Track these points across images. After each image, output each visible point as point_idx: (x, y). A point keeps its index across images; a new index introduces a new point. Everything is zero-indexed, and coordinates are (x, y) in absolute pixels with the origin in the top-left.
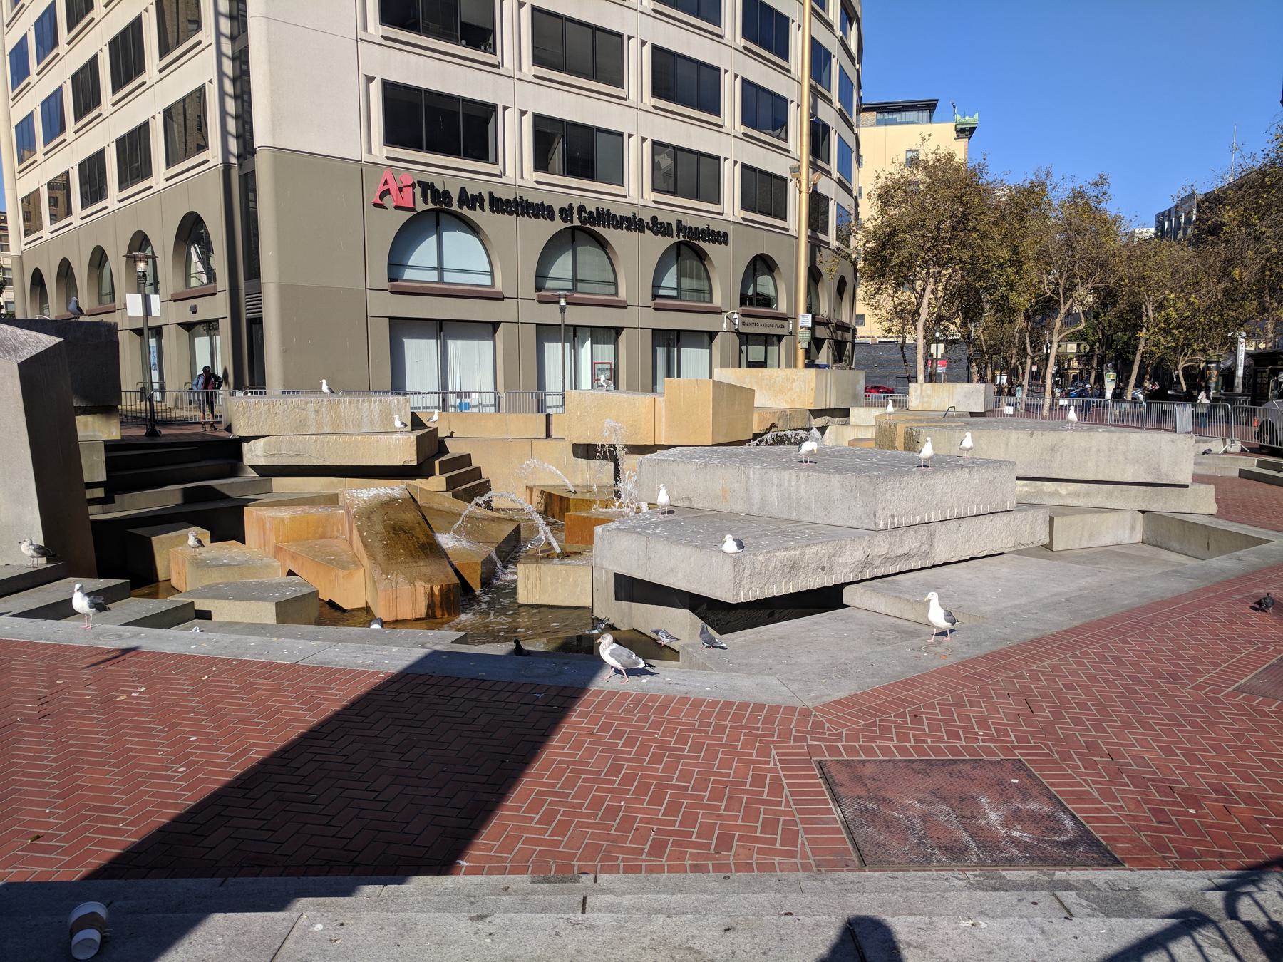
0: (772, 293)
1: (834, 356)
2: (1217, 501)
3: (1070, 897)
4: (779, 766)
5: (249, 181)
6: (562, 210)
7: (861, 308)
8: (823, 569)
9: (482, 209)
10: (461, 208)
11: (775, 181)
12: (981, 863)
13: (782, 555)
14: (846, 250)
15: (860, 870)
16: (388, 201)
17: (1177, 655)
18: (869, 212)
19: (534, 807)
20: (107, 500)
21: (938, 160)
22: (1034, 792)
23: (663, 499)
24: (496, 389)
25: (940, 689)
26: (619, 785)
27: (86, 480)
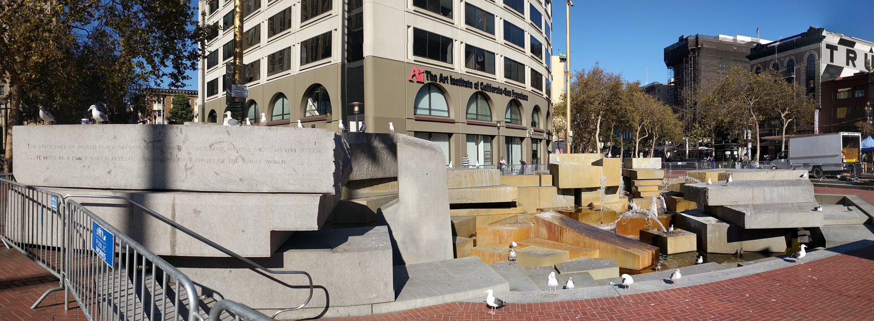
6: (475, 84)
9: (447, 82)
16: (414, 79)
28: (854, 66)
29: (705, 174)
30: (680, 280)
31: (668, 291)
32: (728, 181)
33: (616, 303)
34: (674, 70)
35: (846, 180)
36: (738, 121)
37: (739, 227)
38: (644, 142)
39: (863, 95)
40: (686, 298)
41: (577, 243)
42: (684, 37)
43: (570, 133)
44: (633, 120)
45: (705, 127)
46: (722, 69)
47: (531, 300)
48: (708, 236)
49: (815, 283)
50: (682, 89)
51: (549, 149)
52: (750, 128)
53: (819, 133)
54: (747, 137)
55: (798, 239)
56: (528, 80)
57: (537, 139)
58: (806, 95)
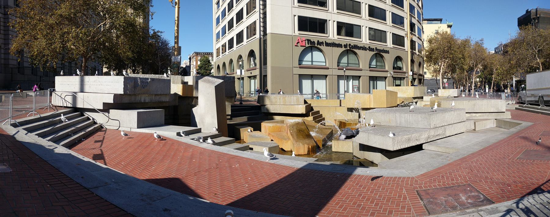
0: (401, 66)
1: (419, 83)
2: (511, 116)
3: (482, 213)
4: (406, 192)
5: (265, 41)
6: (344, 45)
7: (425, 70)
8: (417, 140)
10: (318, 45)
11: (401, 37)
12: (461, 209)
13: (406, 137)
14: (421, 55)
15: (428, 216)
16: (299, 45)
17: (505, 153)
18: (426, 45)
19: (337, 204)
20: (231, 119)
21: (443, 33)
22: (473, 191)
23: (372, 123)
24: (326, 93)
25: (448, 169)
26: (361, 199)
27: (227, 114)
42: (529, 11)
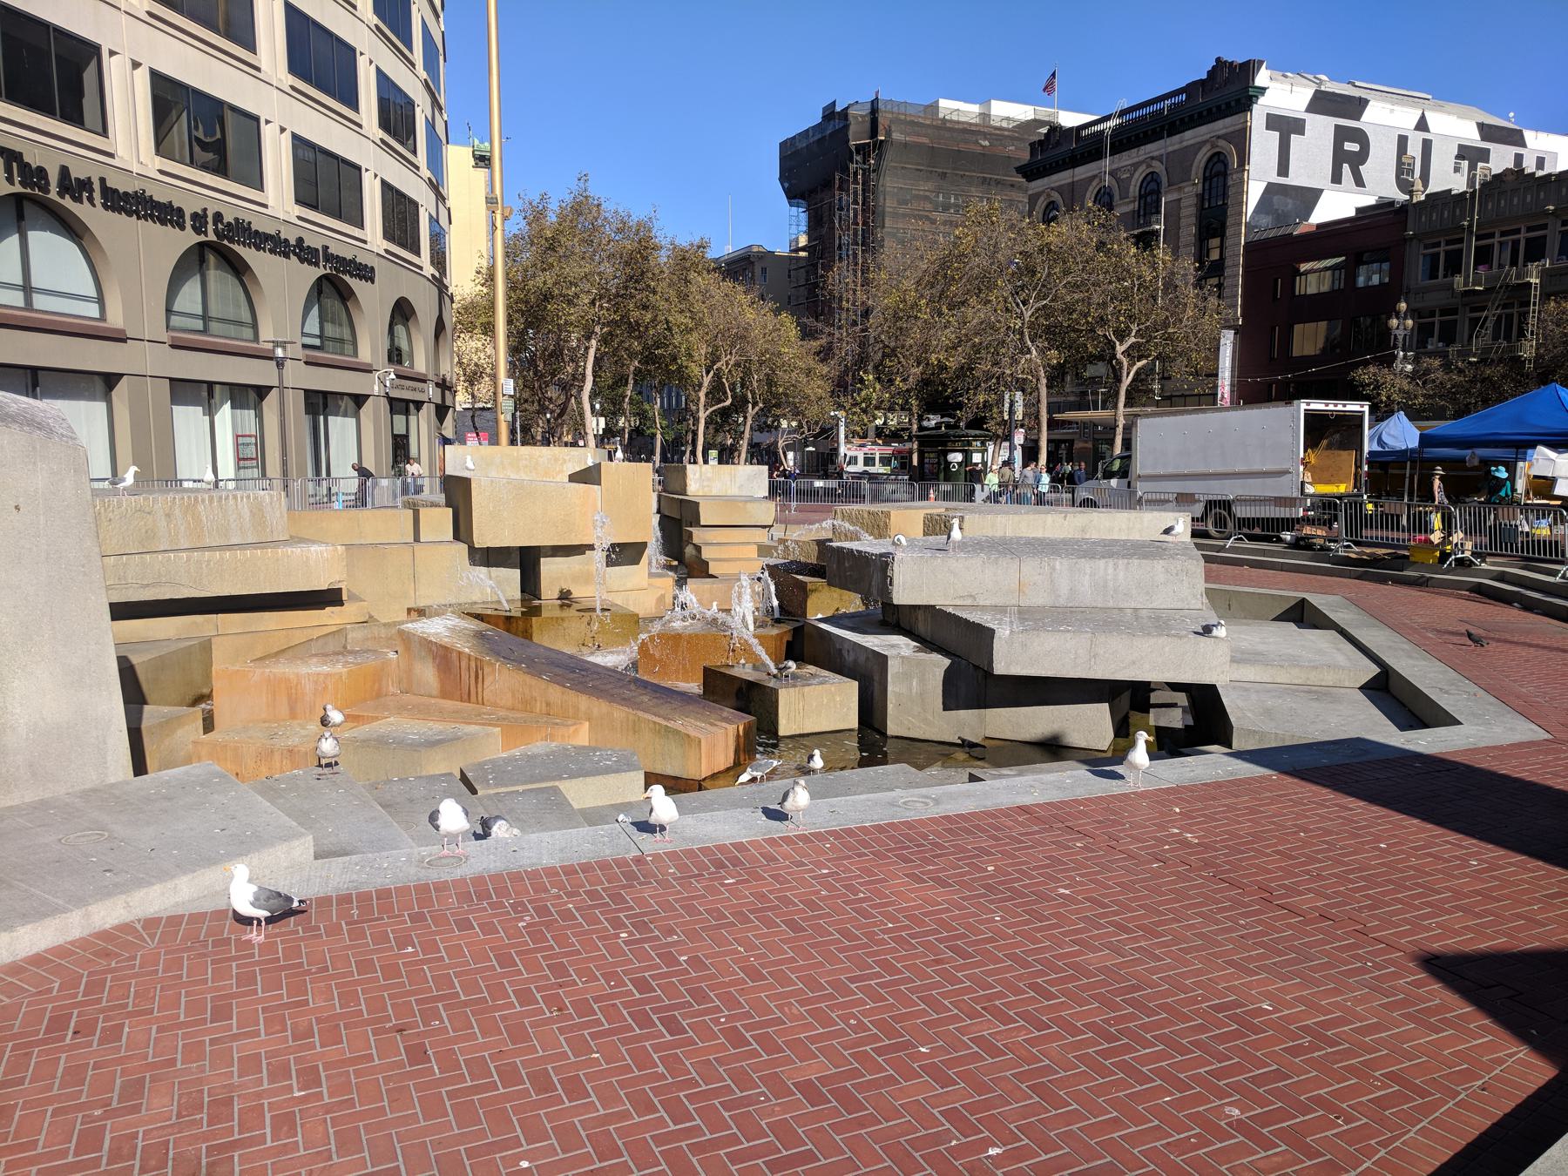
6: (195, 216)
9: (91, 200)
10: (63, 198)
28: (1359, 182)
29: (888, 515)
30: (806, 811)
31: (771, 842)
32: (949, 537)
33: (630, 876)
34: (808, 210)
35: (1309, 547)
36: (985, 366)
37: (976, 667)
38: (721, 421)
39: (1387, 280)
40: (820, 865)
41: (526, 704)
43: (508, 386)
44: (690, 356)
45: (891, 381)
46: (946, 208)
47: (386, 880)
48: (890, 688)
49: (1190, 854)
50: (828, 268)
51: (443, 433)
52: (1022, 386)
53: (1232, 403)
54: (1011, 412)
55: (1151, 715)
56: (373, 216)
57: (407, 402)
58: (1195, 287)
